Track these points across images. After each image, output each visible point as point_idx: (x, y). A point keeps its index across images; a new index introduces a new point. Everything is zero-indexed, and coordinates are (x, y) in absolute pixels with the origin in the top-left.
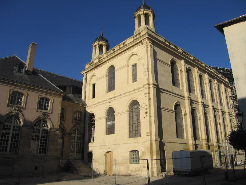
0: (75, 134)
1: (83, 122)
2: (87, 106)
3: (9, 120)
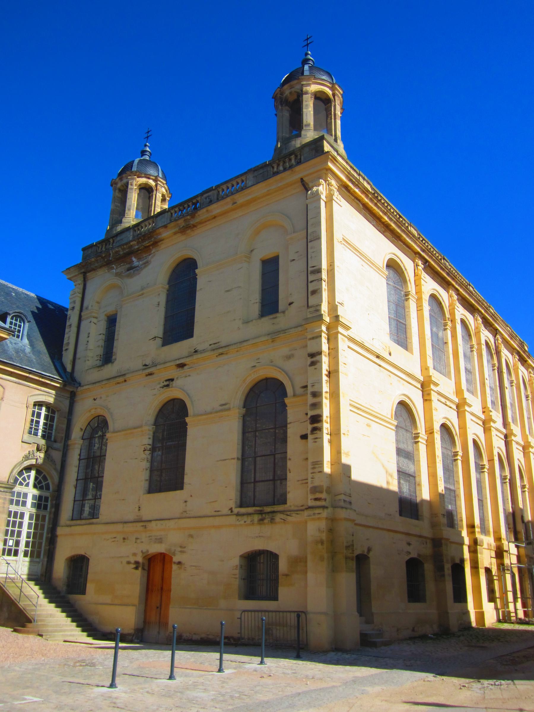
0: (27, 485)
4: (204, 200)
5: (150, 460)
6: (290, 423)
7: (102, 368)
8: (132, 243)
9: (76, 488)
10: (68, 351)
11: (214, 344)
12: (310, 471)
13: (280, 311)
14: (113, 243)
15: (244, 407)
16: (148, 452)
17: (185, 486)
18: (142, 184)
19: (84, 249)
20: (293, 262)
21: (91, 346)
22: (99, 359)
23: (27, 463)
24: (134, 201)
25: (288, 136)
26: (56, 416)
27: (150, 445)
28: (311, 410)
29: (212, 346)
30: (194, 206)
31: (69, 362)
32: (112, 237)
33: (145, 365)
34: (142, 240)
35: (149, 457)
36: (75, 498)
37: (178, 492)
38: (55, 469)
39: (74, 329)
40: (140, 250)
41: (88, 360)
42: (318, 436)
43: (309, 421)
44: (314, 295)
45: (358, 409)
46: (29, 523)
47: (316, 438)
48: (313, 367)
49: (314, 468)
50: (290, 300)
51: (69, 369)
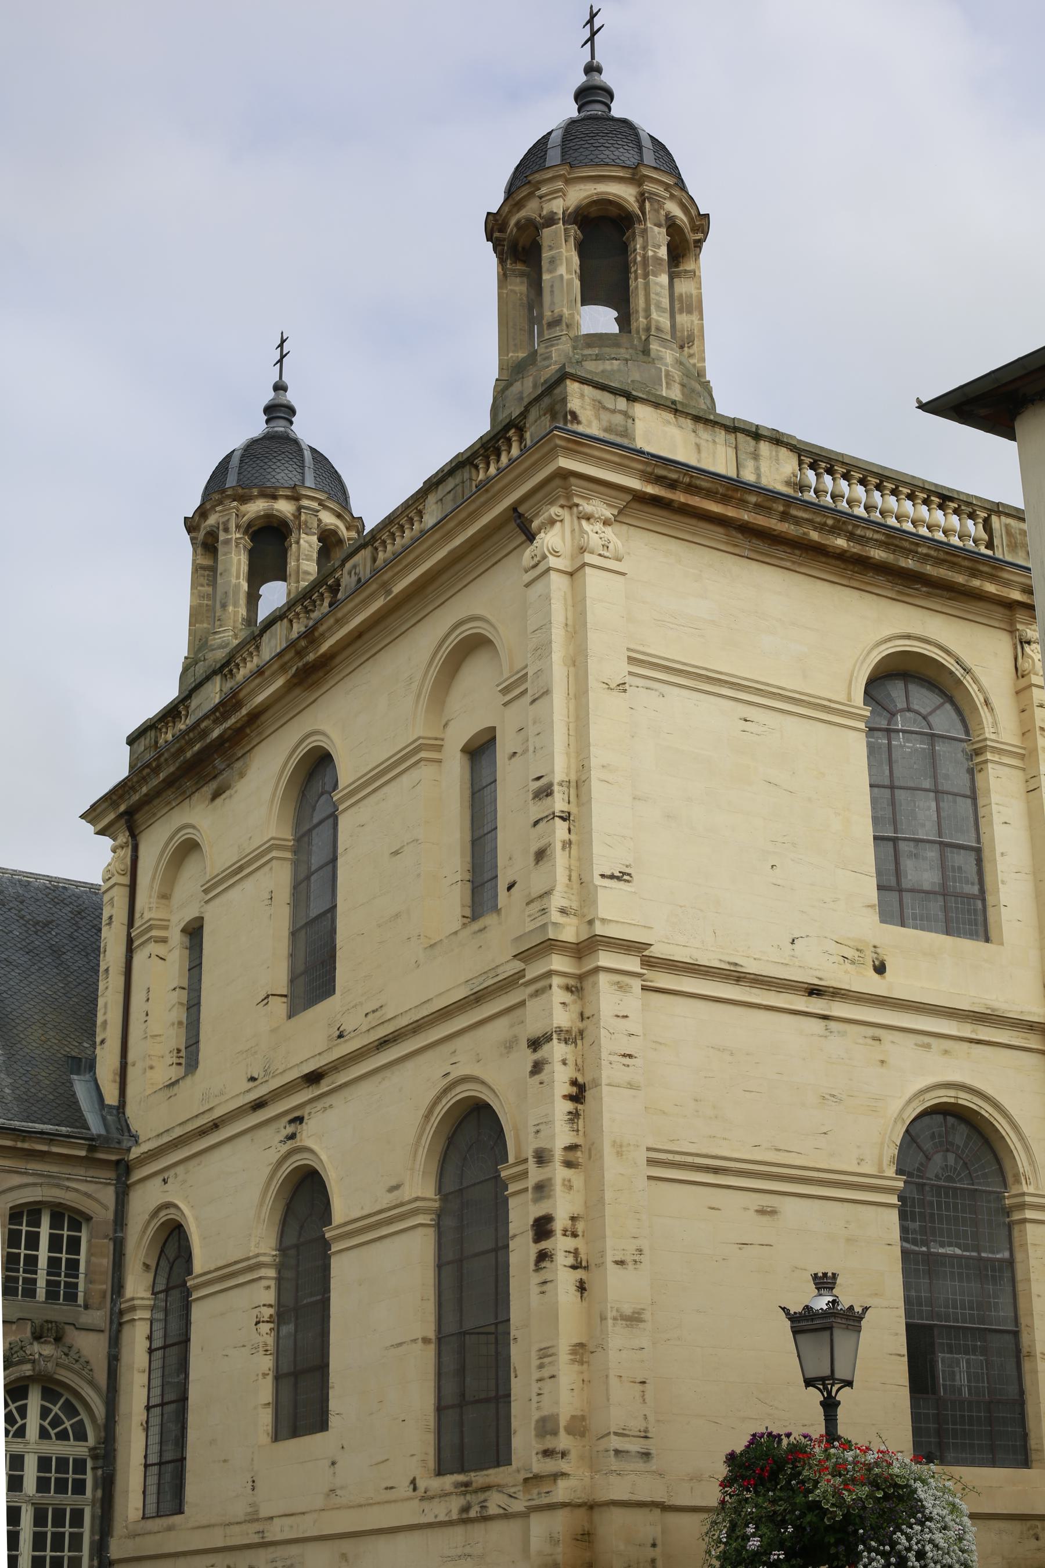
1: (98, 1317)
2: (135, 1152)
5: (271, 1347)
6: (515, 1236)
8: (203, 725)
9: (147, 1430)
11: (374, 1011)
14: (187, 716)
16: (265, 1328)
17: (333, 1421)
18: (259, 517)
24: (238, 577)
27: (270, 1306)
28: (536, 1201)
29: (370, 1016)
31: (111, 1077)
33: (253, 1079)
34: (222, 714)
35: (270, 1340)
36: (146, 1457)
37: (319, 1436)
38: (92, 1383)
40: (228, 740)
41: (151, 1068)
44: (540, 863)
45: (716, 1170)
46: (35, 1534)
47: (545, 1283)
48: (537, 1078)
49: (541, 1366)
51: (111, 1097)
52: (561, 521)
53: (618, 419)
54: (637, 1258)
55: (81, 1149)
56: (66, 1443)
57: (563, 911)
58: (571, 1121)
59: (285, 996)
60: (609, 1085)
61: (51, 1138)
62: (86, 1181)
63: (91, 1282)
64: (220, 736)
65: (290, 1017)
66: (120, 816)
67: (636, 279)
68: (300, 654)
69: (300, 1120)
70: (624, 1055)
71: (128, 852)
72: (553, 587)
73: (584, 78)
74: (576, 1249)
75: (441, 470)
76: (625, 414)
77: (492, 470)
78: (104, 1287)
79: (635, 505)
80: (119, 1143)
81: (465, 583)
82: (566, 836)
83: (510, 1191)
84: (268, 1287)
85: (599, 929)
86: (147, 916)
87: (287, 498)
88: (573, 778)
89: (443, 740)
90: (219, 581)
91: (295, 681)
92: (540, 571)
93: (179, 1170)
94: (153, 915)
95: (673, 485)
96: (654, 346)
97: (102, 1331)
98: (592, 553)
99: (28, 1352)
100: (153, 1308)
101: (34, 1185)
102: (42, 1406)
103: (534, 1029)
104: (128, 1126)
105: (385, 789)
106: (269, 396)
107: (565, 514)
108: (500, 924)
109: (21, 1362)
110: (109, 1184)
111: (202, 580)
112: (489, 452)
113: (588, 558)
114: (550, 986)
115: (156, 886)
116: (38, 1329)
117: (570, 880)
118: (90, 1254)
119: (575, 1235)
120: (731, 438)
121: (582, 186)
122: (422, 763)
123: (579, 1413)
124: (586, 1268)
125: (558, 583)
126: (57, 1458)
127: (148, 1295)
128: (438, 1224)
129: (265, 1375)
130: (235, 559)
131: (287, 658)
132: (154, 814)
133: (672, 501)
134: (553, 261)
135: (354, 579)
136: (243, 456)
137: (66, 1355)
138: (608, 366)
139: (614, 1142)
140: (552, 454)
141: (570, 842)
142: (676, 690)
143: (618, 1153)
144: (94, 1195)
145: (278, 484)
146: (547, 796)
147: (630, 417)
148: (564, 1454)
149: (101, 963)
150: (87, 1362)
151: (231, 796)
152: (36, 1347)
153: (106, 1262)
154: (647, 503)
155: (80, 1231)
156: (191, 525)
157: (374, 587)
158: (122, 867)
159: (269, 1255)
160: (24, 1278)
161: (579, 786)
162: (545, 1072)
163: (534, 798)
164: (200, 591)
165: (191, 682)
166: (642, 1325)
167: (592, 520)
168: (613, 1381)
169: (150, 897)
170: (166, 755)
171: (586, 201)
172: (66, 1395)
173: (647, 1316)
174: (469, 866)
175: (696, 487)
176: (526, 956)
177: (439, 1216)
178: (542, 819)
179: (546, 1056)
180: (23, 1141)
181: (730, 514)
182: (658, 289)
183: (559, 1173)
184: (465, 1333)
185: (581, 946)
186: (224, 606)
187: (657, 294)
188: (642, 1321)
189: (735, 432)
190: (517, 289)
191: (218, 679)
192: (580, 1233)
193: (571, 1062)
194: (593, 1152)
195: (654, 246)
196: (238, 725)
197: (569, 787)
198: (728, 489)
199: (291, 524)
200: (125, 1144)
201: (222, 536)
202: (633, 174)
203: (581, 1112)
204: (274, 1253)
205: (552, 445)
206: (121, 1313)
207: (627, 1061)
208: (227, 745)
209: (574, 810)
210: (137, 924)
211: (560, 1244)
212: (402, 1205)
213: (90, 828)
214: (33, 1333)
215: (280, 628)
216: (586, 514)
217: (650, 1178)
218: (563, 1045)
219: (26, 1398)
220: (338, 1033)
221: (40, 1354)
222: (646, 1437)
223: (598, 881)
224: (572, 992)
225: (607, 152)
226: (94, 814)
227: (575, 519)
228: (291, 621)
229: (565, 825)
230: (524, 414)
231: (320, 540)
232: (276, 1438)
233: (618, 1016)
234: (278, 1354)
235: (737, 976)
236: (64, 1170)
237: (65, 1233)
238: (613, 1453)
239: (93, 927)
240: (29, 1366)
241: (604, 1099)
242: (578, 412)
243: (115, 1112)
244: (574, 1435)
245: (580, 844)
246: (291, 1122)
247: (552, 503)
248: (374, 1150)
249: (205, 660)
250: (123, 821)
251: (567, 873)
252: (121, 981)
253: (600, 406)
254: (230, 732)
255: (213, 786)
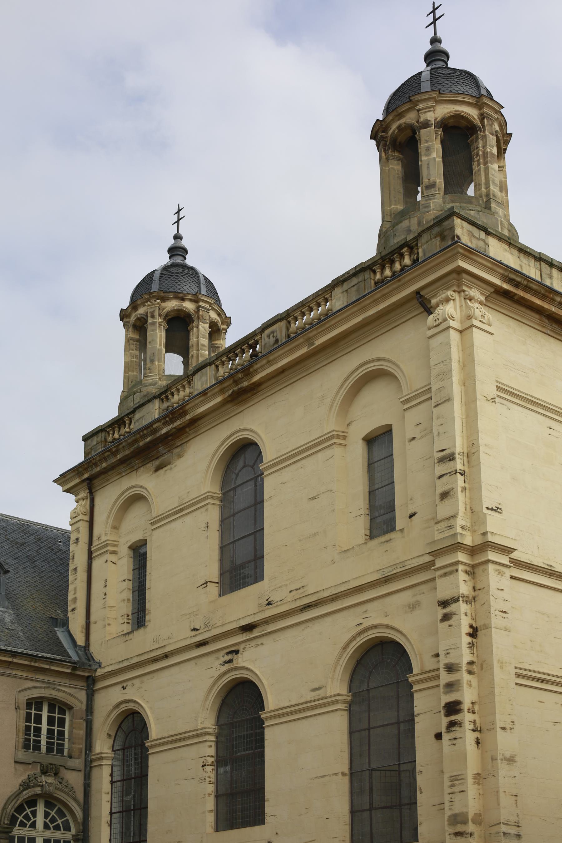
0: (33, 825)
1: (78, 763)
2: (100, 672)
3: (27, 817)
4: (267, 339)
6: (419, 714)
7: (131, 636)
8: (155, 426)
10: (76, 612)
11: (297, 590)
12: (447, 790)
13: (397, 528)
14: (130, 424)
15: (350, 692)
17: (268, 819)
18: (173, 311)
19: (86, 439)
20: (413, 442)
21: (110, 601)
22: (126, 621)
23: (26, 794)
24: (160, 345)
25: (400, 207)
26: (67, 718)
27: (212, 756)
28: (446, 693)
29: (294, 593)
30: (251, 351)
31: (80, 629)
32: (128, 415)
33: (195, 630)
34: (170, 419)
35: (213, 776)
37: (257, 828)
38: (75, 799)
39: (82, 575)
40: (171, 435)
41: (109, 625)
42: (457, 735)
43: (443, 712)
44: (445, 500)
45: (542, 681)
47: (455, 739)
48: (446, 623)
49: (452, 786)
50: (411, 511)
51: (80, 640)
52: (453, 300)
53: (481, 244)
54: (511, 726)
55: (68, 668)
56: (59, 832)
57: (463, 527)
58: (470, 648)
59: (217, 583)
60: (495, 628)
61: (51, 661)
62: (70, 687)
63: (73, 743)
64: (167, 432)
65: (220, 595)
66: (83, 481)
67: (479, 165)
68: (236, 382)
69: (237, 652)
70: (502, 612)
71: (87, 503)
72: (452, 338)
73: (430, 47)
74: (475, 720)
75: (348, 273)
76: (484, 241)
77: (388, 272)
78: (81, 746)
79: (494, 296)
80: (90, 666)
81: (374, 337)
82: (463, 485)
83: (414, 689)
84: (211, 746)
85: (490, 538)
86: (104, 538)
87: (191, 300)
88: (466, 451)
89: (347, 433)
90: (149, 346)
91: (229, 399)
92: (442, 327)
93: (137, 682)
94: (108, 538)
95: (517, 285)
96: (493, 205)
97: (80, 771)
98: (476, 319)
99: (39, 781)
100: (113, 759)
101: (40, 687)
102: (45, 811)
103: (443, 593)
104: (92, 657)
105: (303, 462)
106: (171, 242)
107: (456, 295)
108: (403, 537)
109: (35, 786)
110: (83, 689)
111: (132, 346)
112: (385, 262)
113: (475, 322)
114: (457, 571)
115: (111, 521)
116: (45, 768)
117: (466, 510)
118: (71, 726)
119: (474, 713)
120: (538, 264)
121: (445, 106)
122: (335, 446)
123: (478, 812)
124: (480, 731)
125: (454, 336)
126: (54, 840)
127: (110, 751)
128: (350, 709)
129: (209, 795)
130: (159, 334)
131: (226, 384)
132: (108, 480)
133: (516, 294)
134: (428, 149)
135: (272, 340)
136: (161, 274)
137: (60, 783)
138: (472, 213)
139: (499, 660)
140: (454, 257)
141: (465, 488)
142: (516, 407)
143: (501, 666)
144: (76, 696)
145: (184, 292)
146: (450, 460)
147: (487, 244)
148: (471, 835)
149: (70, 565)
150: (72, 788)
151: (171, 469)
152: (43, 778)
153: (82, 733)
154: (501, 295)
155: (65, 715)
156: (124, 315)
157: (301, 340)
158: (85, 510)
159: (211, 728)
160: (34, 740)
161: (471, 455)
162: (453, 619)
163: (438, 462)
164: (131, 353)
165: (131, 405)
166: (515, 764)
167: (473, 301)
168: (501, 794)
169: (106, 527)
170: (124, 444)
171: (448, 115)
172: (59, 806)
173: (517, 759)
174: (368, 506)
175: (530, 288)
176: (437, 553)
177: (350, 705)
178: (446, 474)
179: (454, 610)
180: (35, 662)
181: (546, 307)
182: (493, 172)
183: (466, 677)
184: (372, 770)
185: (474, 548)
186: (152, 361)
187: (493, 175)
188: (515, 761)
189: (540, 261)
190: (395, 167)
191: (157, 402)
192: (476, 712)
193: (469, 614)
194: (484, 666)
195: (490, 146)
196: (181, 426)
197: (463, 456)
198: (546, 291)
199: (193, 316)
200: (94, 667)
201: (150, 320)
202: (477, 102)
203: (475, 643)
204: (215, 727)
205: (455, 251)
206: (91, 761)
207: (504, 615)
208: (170, 438)
209: (467, 470)
210: (94, 544)
211: (466, 718)
212: (325, 698)
213: (60, 488)
214: (41, 770)
215: (209, 371)
216: (470, 296)
217: (517, 684)
218: (465, 604)
219: (36, 806)
220: (267, 602)
221: (46, 782)
222: (518, 826)
223: (485, 511)
224: (469, 574)
225: (460, 87)
226: (64, 479)
227: (463, 299)
228: (217, 367)
229: (462, 478)
230: (416, 239)
231: (209, 328)
232: (217, 829)
233: (498, 589)
234: (217, 783)
235: (550, 573)
236: (57, 680)
237: (57, 715)
238: (502, 834)
239: (49, 548)
240: (39, 789)
241: (493, 636)
242: (461, 236)
243: (83, 649)
244: (476, 824)
245: (474, 489)
246: (228, 653)
247: (447, 289)
248: (301, 669)
249: (141, 392)
250: (85, 484)
251: (464, 506)
252: (85, 576)
253: (471, 235)
254: (174, 430)
255: (157, 463)
